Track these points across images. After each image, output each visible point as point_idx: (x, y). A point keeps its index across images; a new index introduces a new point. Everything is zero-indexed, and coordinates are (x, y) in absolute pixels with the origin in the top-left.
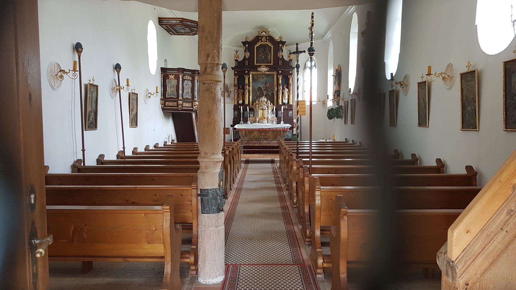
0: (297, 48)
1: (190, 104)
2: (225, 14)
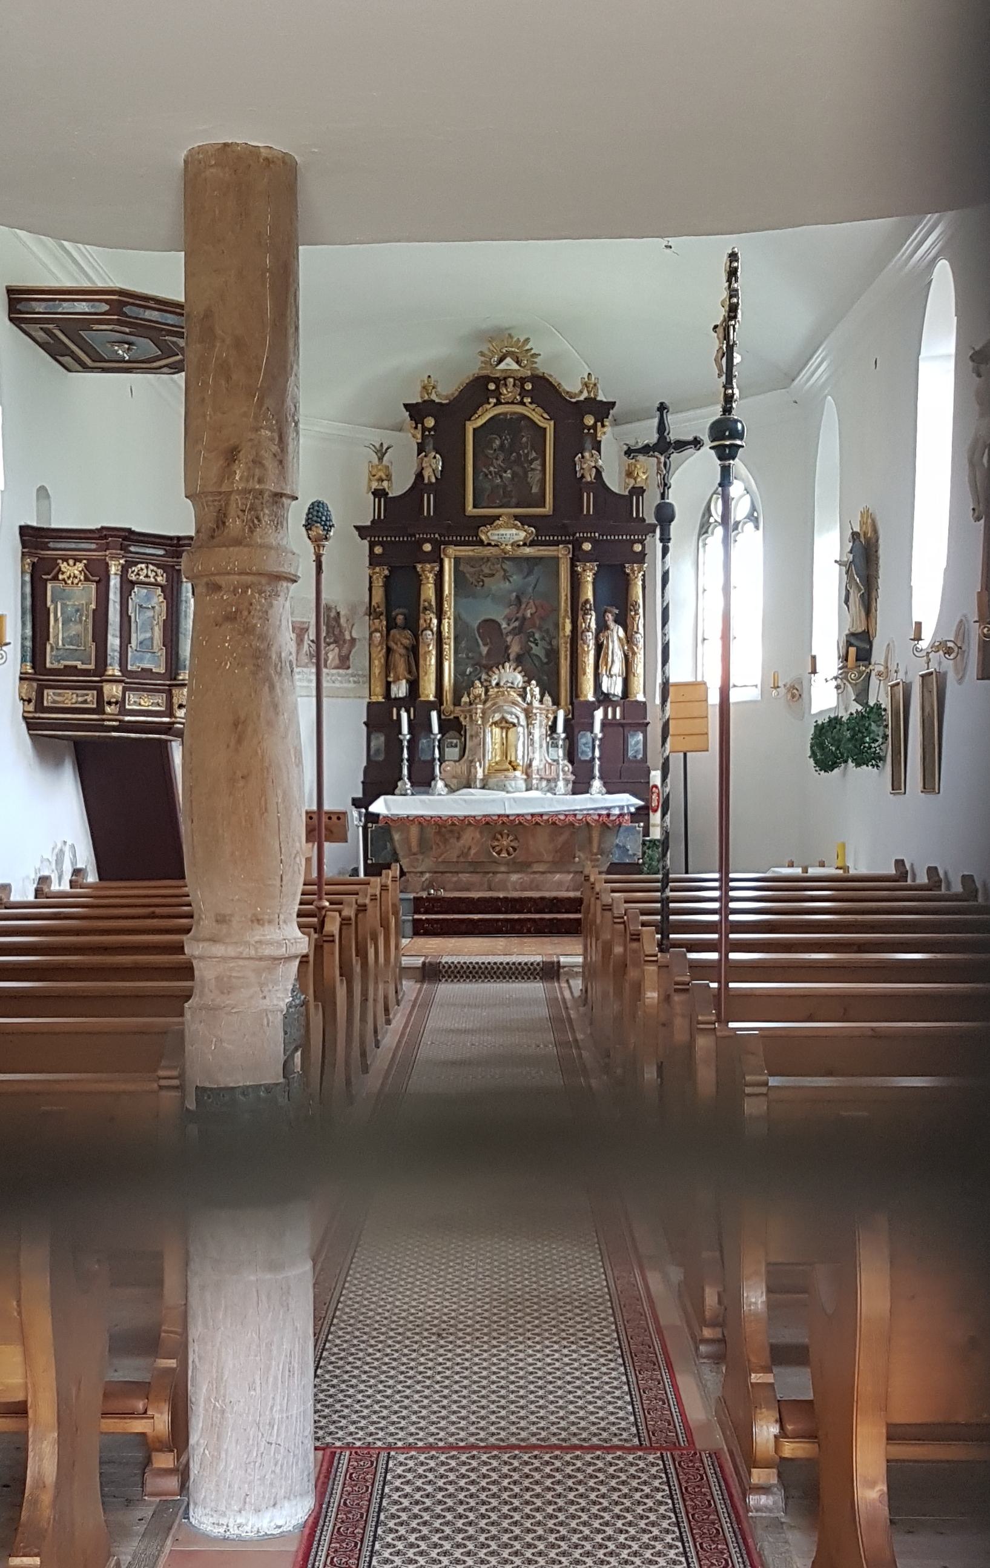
0: (662, 428)
1: (161, 698)
2: (311, 260)
